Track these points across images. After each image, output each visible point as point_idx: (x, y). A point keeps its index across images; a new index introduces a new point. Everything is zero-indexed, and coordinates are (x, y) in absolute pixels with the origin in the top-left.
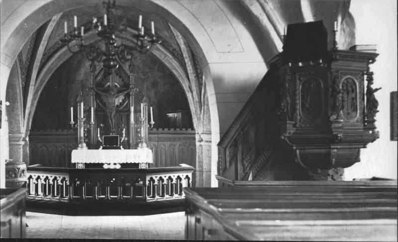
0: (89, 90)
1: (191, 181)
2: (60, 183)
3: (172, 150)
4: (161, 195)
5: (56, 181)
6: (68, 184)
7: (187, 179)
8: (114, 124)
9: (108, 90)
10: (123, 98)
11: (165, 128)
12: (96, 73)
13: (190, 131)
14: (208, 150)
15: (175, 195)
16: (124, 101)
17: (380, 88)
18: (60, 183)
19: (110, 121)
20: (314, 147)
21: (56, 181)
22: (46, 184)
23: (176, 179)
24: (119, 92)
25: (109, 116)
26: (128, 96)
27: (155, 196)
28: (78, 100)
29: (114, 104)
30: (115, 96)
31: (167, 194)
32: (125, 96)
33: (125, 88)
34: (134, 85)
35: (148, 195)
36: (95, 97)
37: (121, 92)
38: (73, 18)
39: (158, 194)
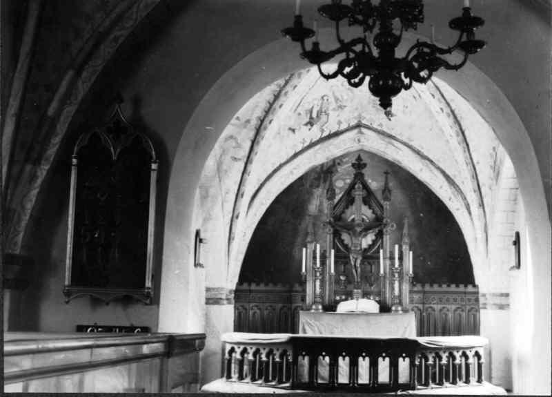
0: (324, 225)
1: (483, 360)
2: (264, 358)
3: (444, 316)
4: (437, 381)
5: (271, 358)
6: (291, 360)
7: (476, 358)
8: (359, 276)
9: (350, 228)
10: (374, 238)
11: (453, 283)
12: (336, 201)
13: (470, 288)
14: (120, 331)
15: (445, 382)
16: (374, 242)
17: (487, 256)
18: (278, 360)
19: (354, 271)
20: (56, 336)
21: (271, 358)
22: (282, 362)
23: (447, 357)
24: (367, 229)
25: (353, 263)
26: (380, 235)
27: (443, 383)
28: (309, 239)
29: (361, 245)
30: (362, 235)
31: (446, 381)
32: (376, 235)
33: (378, 223)
34: (389, 218)
35: (460, 380)
36: (332, 236)
37: (370, 229)
38: (400, 75)
39: (434, 381)
